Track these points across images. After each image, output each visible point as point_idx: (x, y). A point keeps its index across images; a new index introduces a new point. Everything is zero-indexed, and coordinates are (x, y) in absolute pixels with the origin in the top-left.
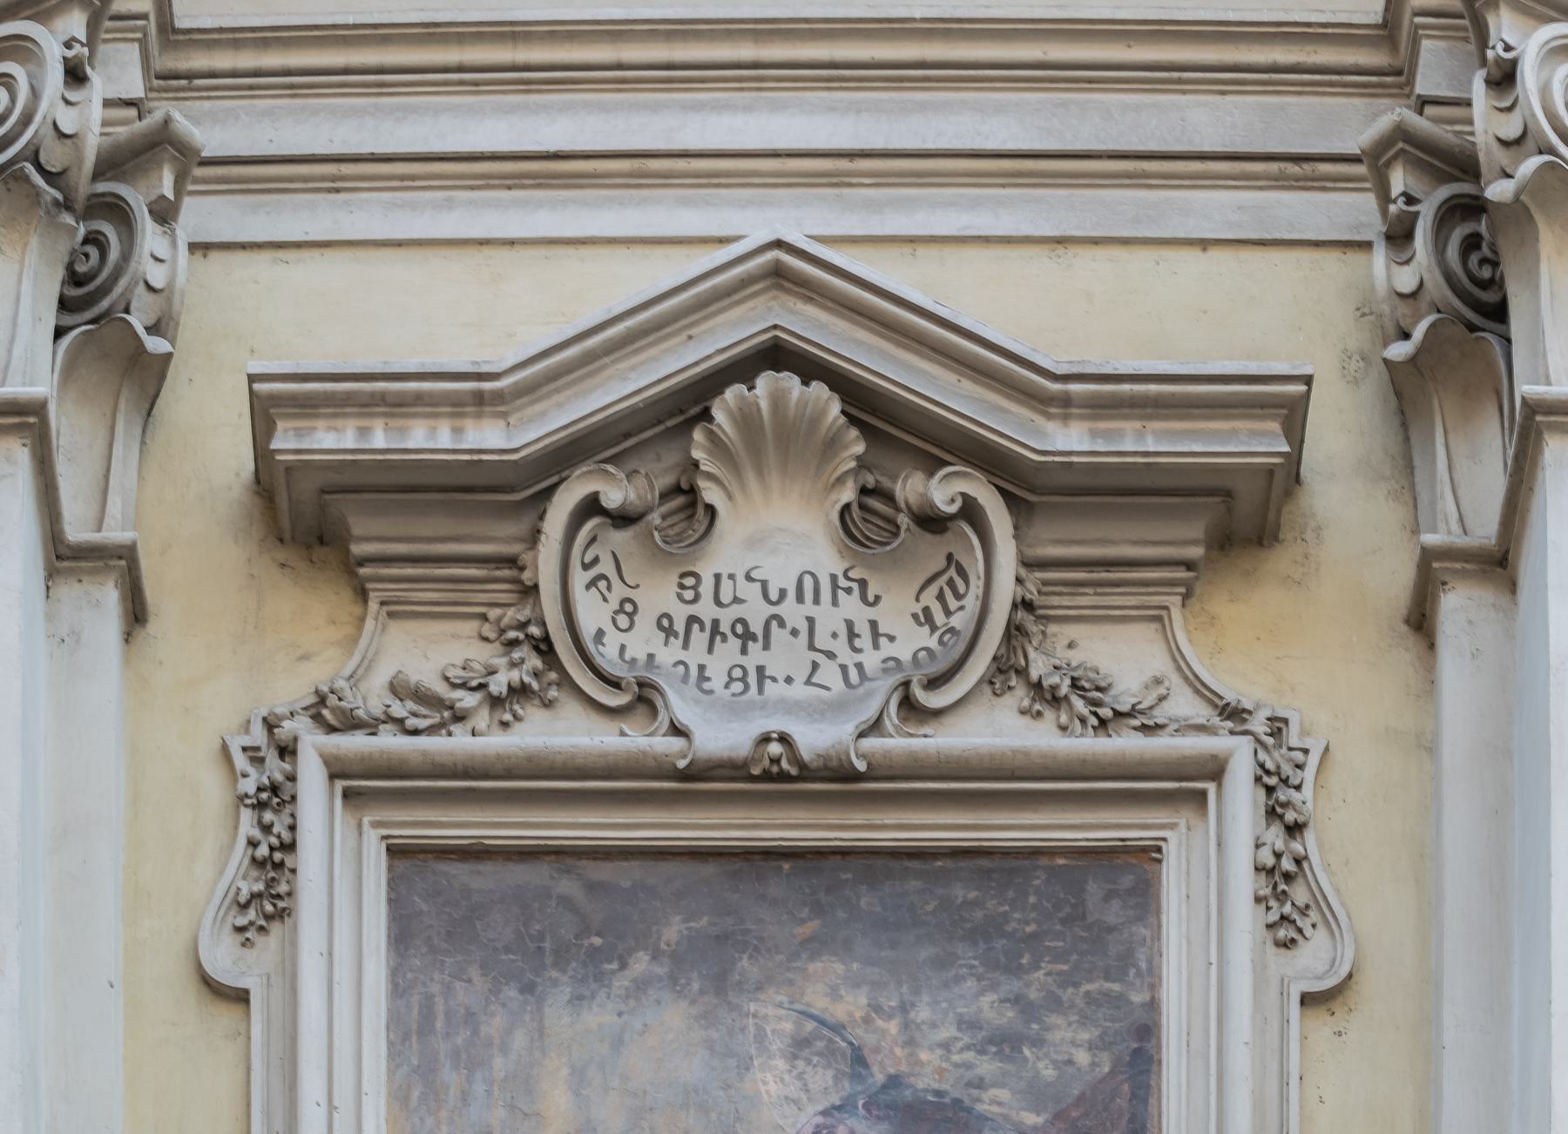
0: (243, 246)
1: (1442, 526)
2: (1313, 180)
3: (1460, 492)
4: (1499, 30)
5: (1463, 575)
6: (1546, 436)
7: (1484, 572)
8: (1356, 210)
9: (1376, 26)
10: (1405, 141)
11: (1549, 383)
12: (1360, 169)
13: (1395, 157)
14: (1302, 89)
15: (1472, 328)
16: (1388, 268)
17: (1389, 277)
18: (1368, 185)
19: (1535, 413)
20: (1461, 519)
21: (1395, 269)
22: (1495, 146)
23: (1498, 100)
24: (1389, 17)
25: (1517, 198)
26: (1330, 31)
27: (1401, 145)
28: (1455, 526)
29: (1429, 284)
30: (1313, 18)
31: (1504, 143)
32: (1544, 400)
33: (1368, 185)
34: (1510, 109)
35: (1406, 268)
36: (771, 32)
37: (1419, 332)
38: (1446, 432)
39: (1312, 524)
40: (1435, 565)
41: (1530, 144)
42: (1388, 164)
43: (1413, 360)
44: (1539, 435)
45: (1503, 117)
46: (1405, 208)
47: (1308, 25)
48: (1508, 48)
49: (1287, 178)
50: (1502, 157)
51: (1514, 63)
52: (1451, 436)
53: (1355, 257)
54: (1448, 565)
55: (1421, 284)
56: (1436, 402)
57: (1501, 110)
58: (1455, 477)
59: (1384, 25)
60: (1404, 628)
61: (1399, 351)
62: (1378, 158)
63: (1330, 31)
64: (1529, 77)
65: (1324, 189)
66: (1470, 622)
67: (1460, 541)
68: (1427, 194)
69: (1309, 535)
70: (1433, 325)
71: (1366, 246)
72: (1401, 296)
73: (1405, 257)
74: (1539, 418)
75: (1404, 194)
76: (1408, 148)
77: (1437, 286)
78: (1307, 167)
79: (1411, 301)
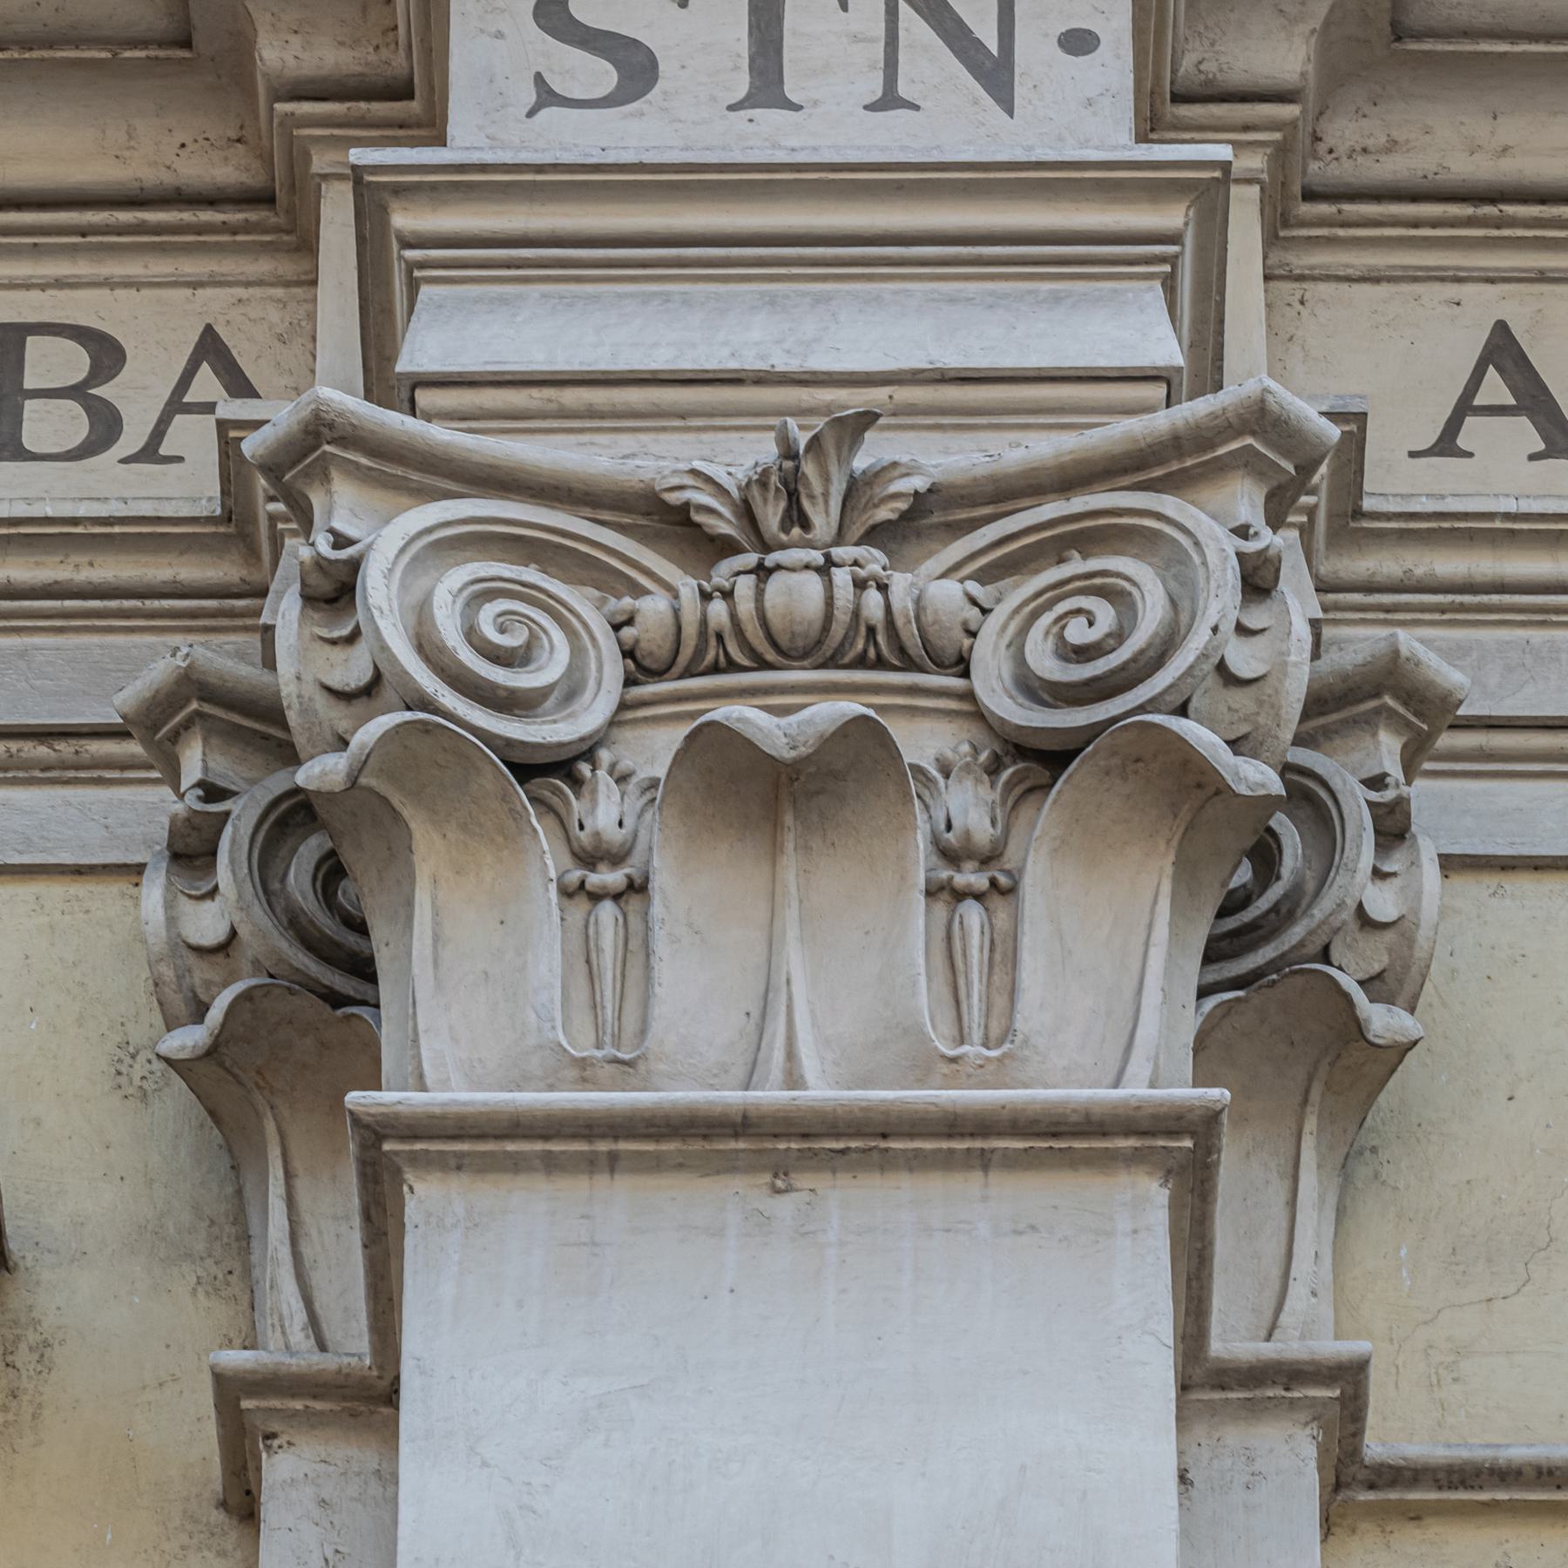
0: (770, 945)
1: (274, 1340)
2: (77, 768)
3: (317, 1278)
4: (329, 514)
5: (312, 1421)
6: (409, 1176)
7: (354, 1415)
8: (143, 812)
9: (209, 520)
10: (202, 699)
11: (424, 1089)
12: (134, 748)
13: (187, 725)
14: (64, 623)
15: (336, 1000)
16: (169, 905)
17: (172, 921)
18: (156, 775)
19: (381, 1138)
20: (314, 1321)
21: (186, 906)
22: (321, 702)
23: (329, 625)
24: (231, 502)
25: (353, 781)
26: (117, 529)
27: (194, 705)
28: (298, 1336)
29: (243, 931)
30: (82, 510)
31: (344, 696)
32: (397, 1116)
33: (156, 775)
34: (353, 638)
35: (208, 905)
36: (1403, 534)
37: (216, 1014)
38: (289, 1176)
39: (32, 1337)
40: (246, 1404)
41: (388, 694)
42: (175, 737)
43: (212, 1052)
44: (397, 1173)
45: (337, 654)
46: (199, 806)
47: (75, 521)
48: (341, 541)
49: (26, 765)
50: (335, 715)
51: (355, 565)
52: (301, 1185)
53: (110, 892)
54: (275, 1403)
55: (233, 933)
56: (270, 1127)
57: (333, 642)
58: (307, 1250)
59: (227, 518)
60: (218, 1516)
61: (189, 1039)
62: (159, 724)
63: (117, 529)
64: (379, 588)
65: (100, 782)
66: (323, 1503)
67: (306, 1359)
68: (253, 782)
69: (23, 1357)
70: (246, 996)
71: (136, 871)
72: (199, 950)
73: (206, 887)
74: (387, 1147)
75: (200, 784)
76: (207, 708)
77: (264, 936)
78: (65, 748)
79: (220, 958)
